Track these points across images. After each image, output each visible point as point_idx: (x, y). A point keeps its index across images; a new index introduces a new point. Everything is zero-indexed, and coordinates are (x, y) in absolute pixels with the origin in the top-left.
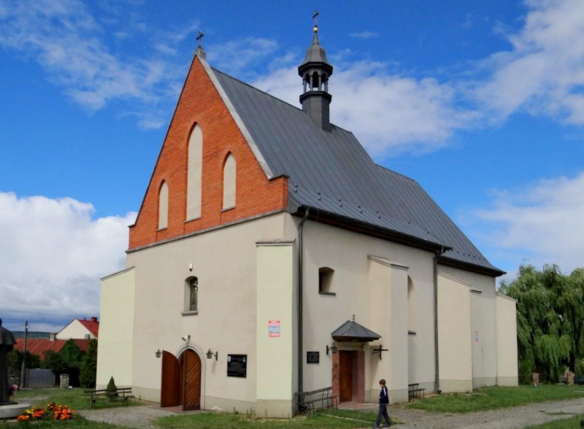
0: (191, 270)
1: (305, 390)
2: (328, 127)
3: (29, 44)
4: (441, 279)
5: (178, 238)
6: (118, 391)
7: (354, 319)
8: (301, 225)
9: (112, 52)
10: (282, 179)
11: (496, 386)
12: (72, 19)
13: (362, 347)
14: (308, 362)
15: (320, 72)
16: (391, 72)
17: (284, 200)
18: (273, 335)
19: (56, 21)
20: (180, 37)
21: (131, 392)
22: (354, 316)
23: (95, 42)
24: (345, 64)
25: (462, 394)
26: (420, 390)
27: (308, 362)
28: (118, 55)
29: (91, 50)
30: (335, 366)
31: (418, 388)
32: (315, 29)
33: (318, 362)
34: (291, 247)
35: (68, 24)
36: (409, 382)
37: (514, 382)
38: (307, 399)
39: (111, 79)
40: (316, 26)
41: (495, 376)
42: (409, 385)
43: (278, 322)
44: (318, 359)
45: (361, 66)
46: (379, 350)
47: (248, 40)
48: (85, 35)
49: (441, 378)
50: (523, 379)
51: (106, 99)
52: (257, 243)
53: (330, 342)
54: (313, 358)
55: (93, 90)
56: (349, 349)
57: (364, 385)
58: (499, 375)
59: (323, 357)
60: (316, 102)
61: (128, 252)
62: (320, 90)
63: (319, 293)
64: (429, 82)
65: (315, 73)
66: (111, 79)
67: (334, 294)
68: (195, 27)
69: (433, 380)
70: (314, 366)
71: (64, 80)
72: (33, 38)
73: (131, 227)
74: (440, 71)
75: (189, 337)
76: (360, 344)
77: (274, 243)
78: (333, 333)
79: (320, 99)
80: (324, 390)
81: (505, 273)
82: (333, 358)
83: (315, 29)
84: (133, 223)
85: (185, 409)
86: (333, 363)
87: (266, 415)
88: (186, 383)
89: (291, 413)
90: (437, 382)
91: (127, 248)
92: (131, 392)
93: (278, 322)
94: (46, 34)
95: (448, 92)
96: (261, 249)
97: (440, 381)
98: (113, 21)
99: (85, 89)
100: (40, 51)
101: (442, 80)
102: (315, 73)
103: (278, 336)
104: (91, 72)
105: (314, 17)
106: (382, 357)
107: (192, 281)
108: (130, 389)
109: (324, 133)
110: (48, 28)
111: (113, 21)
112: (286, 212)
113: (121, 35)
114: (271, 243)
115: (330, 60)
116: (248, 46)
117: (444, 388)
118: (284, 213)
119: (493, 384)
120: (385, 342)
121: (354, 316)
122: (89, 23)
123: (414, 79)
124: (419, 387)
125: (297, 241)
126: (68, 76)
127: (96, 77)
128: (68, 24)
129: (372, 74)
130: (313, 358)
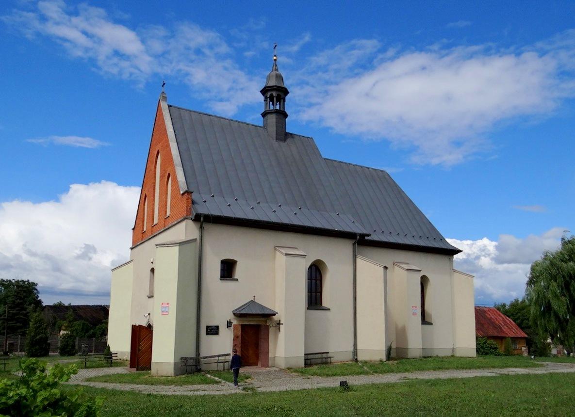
0: (152, 263)
1: (203, 354)
2: (284, 136)
3: (180, 70)
4: (360, 261)
5: (147, 239)
6: (113, 355)
7: (254, 299)
8: (201, 228)
9: (241, 69)
10: (186, 194)
11: (453, 356)
12: (211, 47)
13: (266, 322)
14: (207, 334)
15: (275, 94)
16: (487, 52)
17: (187, 210)
18: (164, 313)
19: (198, 52)
20: (295, 48)
21: (117, 356)
22: (254, 297)
23: (228, 63)
24: (444, 52)
25: (376, 362)
26: (330, 357)
27: (207, 334)
28: (246, 70)
29: (226, 69)
30: (236, 338)
31: (308, 358)
32: (275, 58)
33: (217, 334)
34: (178, 247)
35: (207, 51)
36: (305, 350)
37: (474, 353)
38: (203, 361)
39: (242, 89)
40: (275, 56)
41: (452, 347)
42: (305, 355)
43: (168, 304)
44: (218, 331)
45: (459, 51)
46: (279, 324)
47: (353, 42)
48: (220, 58)
49: (358, 348)
50: (482, 349)
51: (238, 106)
52: (156, 245)
53: (230, 317)
54: (213, 330)
55: (228, 100)
56: (252, 323)
57: (268, 353)
58: (458, 345)
59: (223, 329)
60: (272, 118)
61: (131, 249)
62: (275, 109)
63: (220, 279)
64: (529, 56)
65: (272, 95)
66: (242, 89)
67: (237, 280)
68: (307, 38)
69: (352, 349)
70: (214, 338)
71: (205, 95)
72: (182, 66)
73: (133, 229)
74: (539, 44)
75: (149, 314)
76: (264, 319)
77: (167, 244)
78: (235, 310)
79: (274, 115)
80: (219, 356)
81: (462, 251)
82: (234, 331)
83: (275, 58)
84: (133, 227)
85: (137, 370)
86: (234, 335)
87: (157, 373)
88: (139, 350)
89: (173, 373)
90: (355, 352)
91: (131, 246)
92: (117, 356)
93: (168, 304)
94: (192, 61)
95: (550, 64)
96: (160, 249)
97: (358, 351)
98: (242, 44)
99: (221, 100)
100: (187, 74)
101: (542, 53)
102: (272, 95)
103: (167, 315)
104: (226, 86)
105: (274, 48)
106: (281, 330)
107: (153, 270)
108: (117, 354)
109: (276, 144)
110: (193, 57)
111: (242, 44)
112: (187, 219)
113: (249, 54)
114: (164, 245)
115: (287, 84)
116: (353, 48)
117: (361, 357)
118: (186, 220)
119: (449, 354)
120: (280, 316)
121: (254, 297)
122: (224, 49)
123: (513, 55)
124: (329, 355)
125: (198, 240)
126: (209, 91)
127: (230, 89)
128: (207, 51)
129: (471, 56)
130: (213, 330)
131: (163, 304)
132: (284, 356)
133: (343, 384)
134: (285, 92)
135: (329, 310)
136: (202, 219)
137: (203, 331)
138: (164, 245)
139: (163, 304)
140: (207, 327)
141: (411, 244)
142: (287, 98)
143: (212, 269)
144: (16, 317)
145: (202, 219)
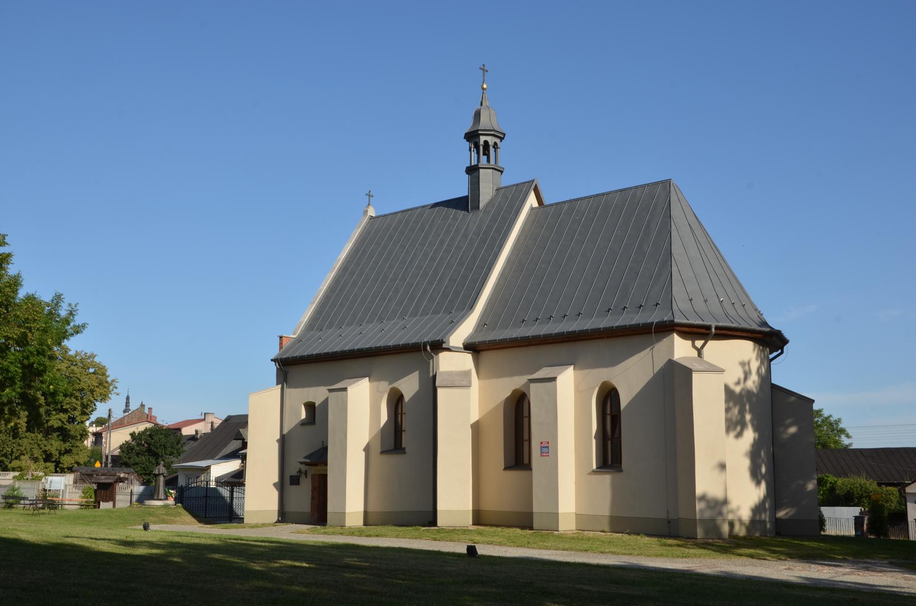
14: (291, 484)
18: (544, 454)
22: (128, 389)
43: (548, 443)
137: (287, 480)
139: (541, 443)
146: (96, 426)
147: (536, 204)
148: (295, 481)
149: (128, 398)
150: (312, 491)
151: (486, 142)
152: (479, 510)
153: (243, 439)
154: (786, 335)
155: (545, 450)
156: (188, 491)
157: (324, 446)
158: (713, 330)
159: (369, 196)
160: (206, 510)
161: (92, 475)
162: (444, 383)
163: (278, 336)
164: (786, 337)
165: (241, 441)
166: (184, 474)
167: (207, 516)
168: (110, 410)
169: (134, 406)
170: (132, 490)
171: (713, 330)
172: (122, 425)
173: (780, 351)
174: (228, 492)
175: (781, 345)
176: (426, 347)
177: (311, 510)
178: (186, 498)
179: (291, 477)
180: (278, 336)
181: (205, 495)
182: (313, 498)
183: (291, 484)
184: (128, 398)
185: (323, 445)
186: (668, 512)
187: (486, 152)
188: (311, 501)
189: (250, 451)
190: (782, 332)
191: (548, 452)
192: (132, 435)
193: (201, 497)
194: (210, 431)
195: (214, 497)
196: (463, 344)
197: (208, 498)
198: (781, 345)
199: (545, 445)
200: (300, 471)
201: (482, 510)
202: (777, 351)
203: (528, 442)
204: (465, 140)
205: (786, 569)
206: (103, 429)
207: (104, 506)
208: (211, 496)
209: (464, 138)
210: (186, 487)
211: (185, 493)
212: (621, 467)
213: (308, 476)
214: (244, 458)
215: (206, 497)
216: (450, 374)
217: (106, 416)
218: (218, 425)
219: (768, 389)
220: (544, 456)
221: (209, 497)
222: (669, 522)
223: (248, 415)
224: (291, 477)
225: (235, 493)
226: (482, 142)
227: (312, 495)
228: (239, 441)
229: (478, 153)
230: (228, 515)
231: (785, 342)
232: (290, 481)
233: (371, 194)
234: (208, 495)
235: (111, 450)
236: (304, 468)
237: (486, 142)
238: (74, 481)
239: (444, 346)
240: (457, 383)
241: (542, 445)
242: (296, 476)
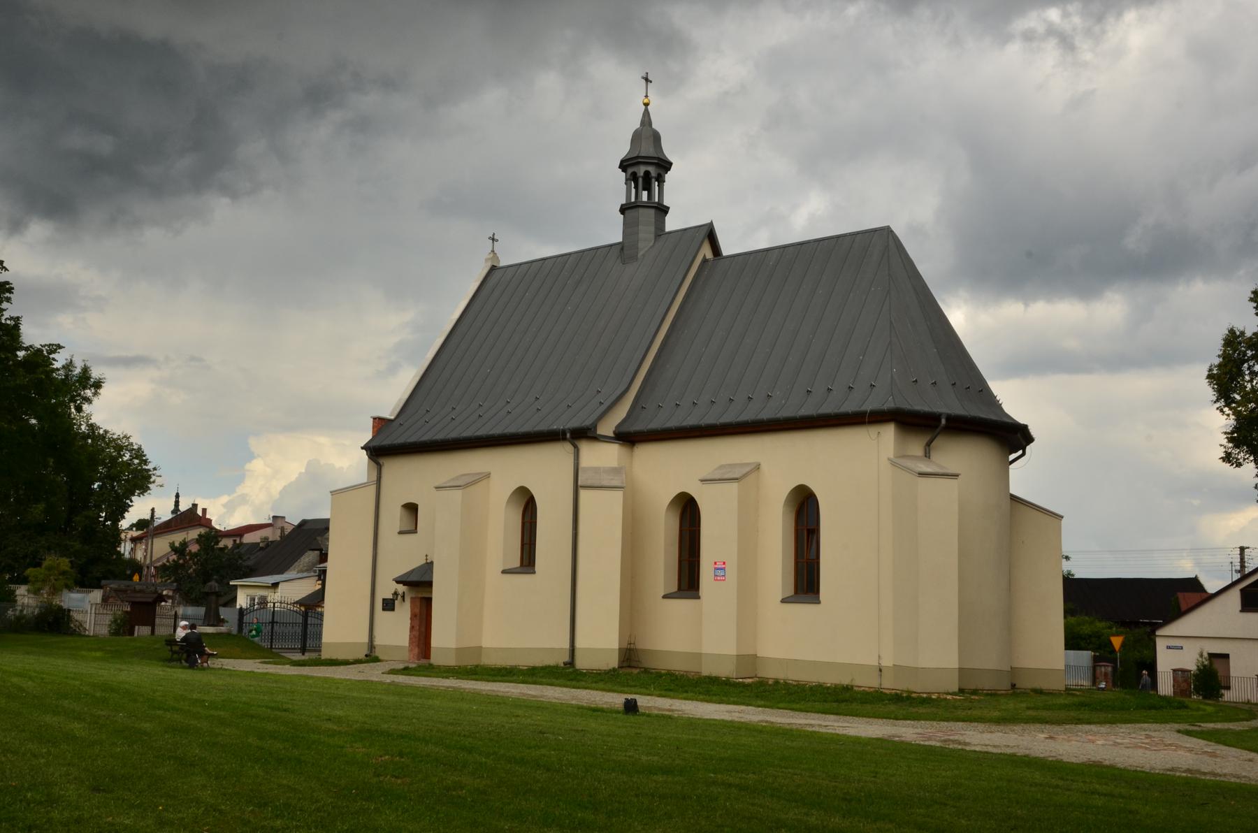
14: (384, 609)
18: (719, 578)
22: (427, 556)
43: (724, 563)
49: (579, 644)
114: (909, 469)
131: (715, 563)
132: (735, 654)
133: (631, 707)
134: (665, 165)
135: (504, 572)
136: (568, 435)
137: (379, 605)
138: (909, 469)
139: (715, 563)
140: (384, 600)
141: (930, 410)
142: (669, 177)
143: (393, 517)
144: (231, 583)
145: (568, 435)
146: (137, 530)
147: (709, 255)
148: (389, 605)
149: (177, 496)
150: (411, 619)
151: (647, 173)
152: (630, 650)
153: (321, 550)
154: (1033, 431)
155: (720, 573)
156: (252, 614)
157: (428, 561)
158: (943, 421)
159: (493, 239)
160: (272, 635)
161: (126, 591)
162: (589, 483)
163: (371, 417)
164: (1032, 434)
165: (317, 553)
166: (245, 593)
167: (274, 647)
168: (702, 481)
169: (183, 507)
170: (176, 612)
171: (943, 421)
172: (168, 528)
173: (1020, 452)
174: (301, 617)
175: (1024, 444)
176: (566, 435)
177: (410, 643)
178: (246, 623)
179: (384, 600)
180: (371, 417)
181: (271, 621)
182: (412, 628)
183: (384, 609)
184: (177, 496)
185: (427, 559)
186: (879, 656)
187: (648, 187)
188: (410, 632)
189: (330, 565)
190: (1029, 428)
191: (724, 576)
192: (172, 545)
193: (266, 623)
194: (279, 539)
195: (283, 623)
196: (614, 432)
197: (275, 624)
198: (1024, 444)
199: (720, 566)
200: (396, 594)
201: (644, 651)
202: (1016, 452)
203: (525, 542)
204: (621, 170)
205: (1047, 738)
206: (145, 533)
207: (142, 631)
208: (279, 621)
209: (619, 167)
210: (247, 609)
211: (245, 617)
212: (819, 597)
213: (406, 600)
214: (322, 575)
215: (273, 622)
216: (596, 470)
217: (148, 517)
218: (289, 531)
219: (1007, 502)
220: (717, 580)
221: (277, 622)
222: (880, 670)
223: (1066, 649)
224: (384, 600)
225: (309, 618)
226: (641, 173)
227: (411, 624)
228: (316, 552)
229: (636, 187)
230: (299, 647)
231: (1029, 439)
232: (383, 606)
233: (650, 78)
234: (275, 620)
235: (153, 559)
236: (401, 588)
237: (647, 173)
238: (103, 599)
239: (589, 435)
240: (605, 483)
241: (716, 566)
242: (391, 599)
